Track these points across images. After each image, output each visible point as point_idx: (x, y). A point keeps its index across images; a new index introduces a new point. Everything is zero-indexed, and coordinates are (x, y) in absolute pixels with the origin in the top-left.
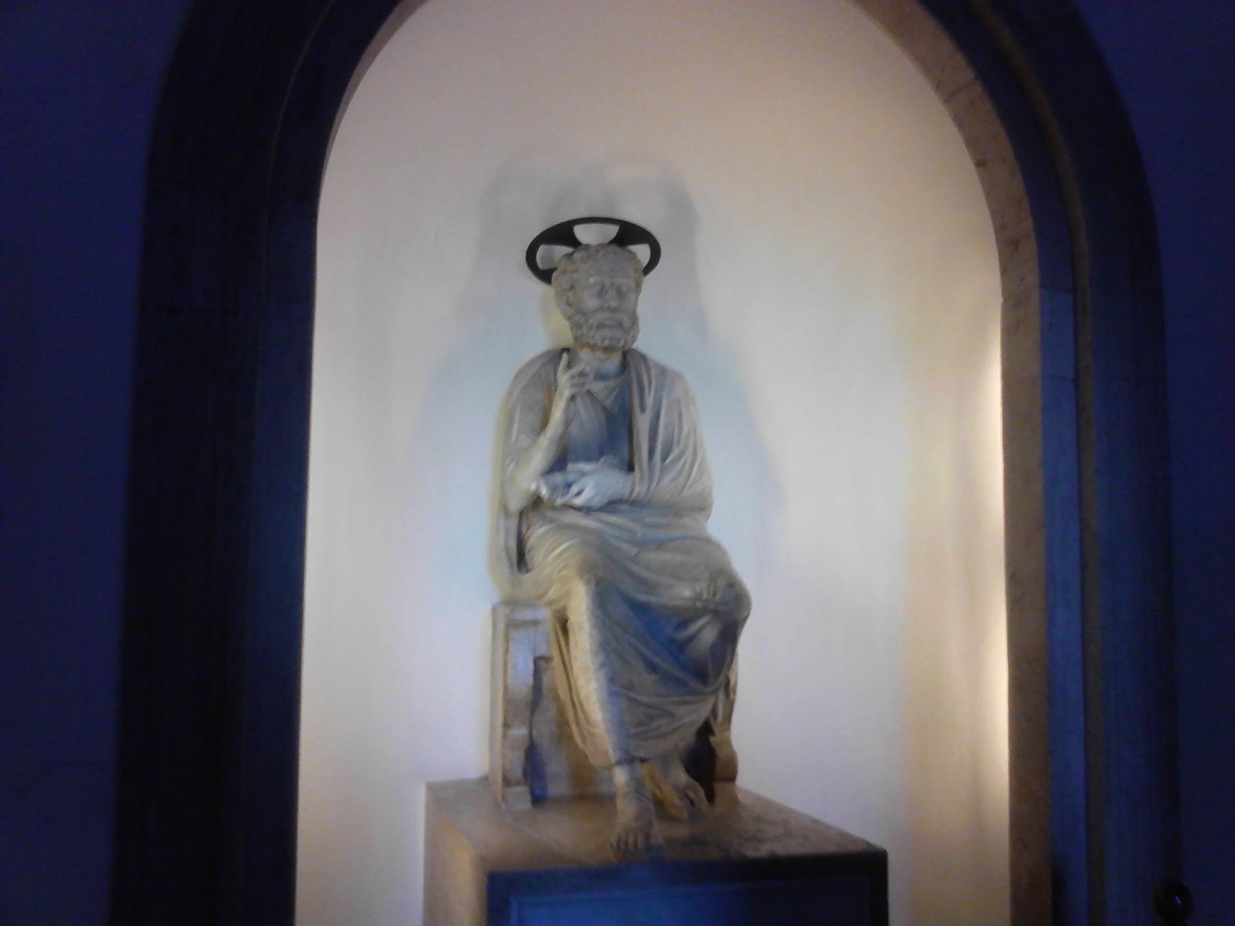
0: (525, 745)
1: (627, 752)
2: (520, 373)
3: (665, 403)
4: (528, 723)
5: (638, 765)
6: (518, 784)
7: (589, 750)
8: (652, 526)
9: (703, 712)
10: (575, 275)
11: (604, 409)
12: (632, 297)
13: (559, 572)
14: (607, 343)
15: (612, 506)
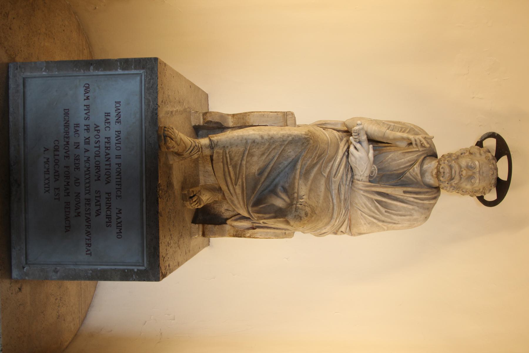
1: (216, 145)
3: (410, 207)
4: (234, 126)
6: (204, 119)
8: (339, 190)
10: (478, 155)
11: (403, 173)
14: (442, 170)
15: (350, 169)
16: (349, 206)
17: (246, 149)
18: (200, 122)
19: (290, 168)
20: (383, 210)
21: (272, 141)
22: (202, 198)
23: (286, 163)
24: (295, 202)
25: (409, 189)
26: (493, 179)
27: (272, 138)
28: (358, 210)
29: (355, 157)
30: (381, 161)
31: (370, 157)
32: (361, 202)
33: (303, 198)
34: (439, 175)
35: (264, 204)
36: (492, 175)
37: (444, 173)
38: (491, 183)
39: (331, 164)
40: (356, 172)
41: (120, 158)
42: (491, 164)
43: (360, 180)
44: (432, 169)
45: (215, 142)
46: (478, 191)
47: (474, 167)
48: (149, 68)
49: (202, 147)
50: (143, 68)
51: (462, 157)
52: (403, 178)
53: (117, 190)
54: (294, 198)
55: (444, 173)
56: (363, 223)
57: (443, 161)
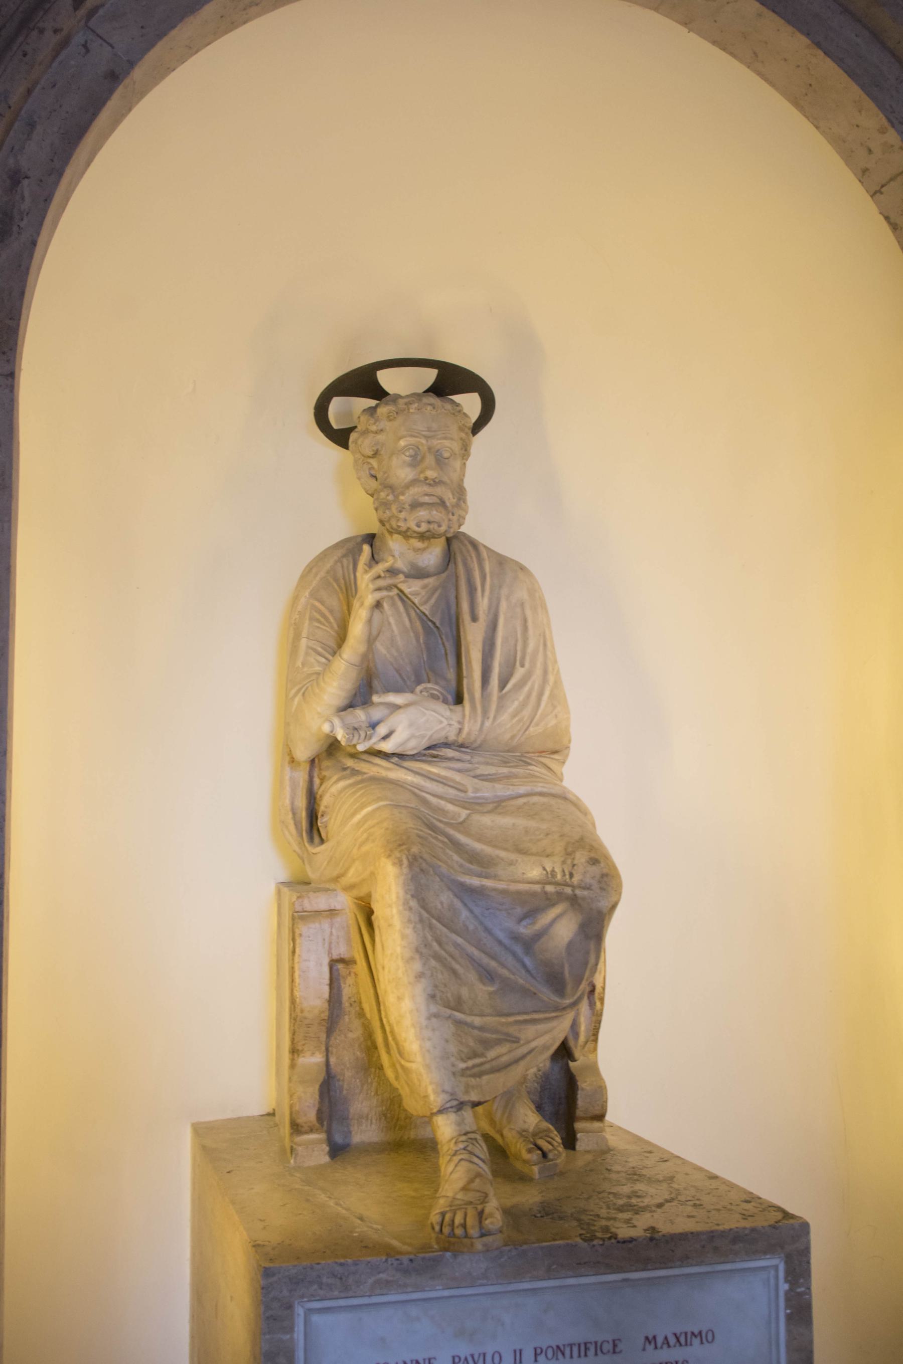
0: (322, 1076)
2: (309, 569)
4: (324, 1048)
5: (468, 1113)
6: (311, 1130)
7: (404, 1091)
9: (558, 1030)
10: (381, 437)
11: (423, 617)
12: (457, 464)
13: (360, 846)
14: (424, 527)
16: (514, 754)
17: (450, 1017)
18: (319, 1142)
19: (475, 902)
20: (519, 673)
21: (424, 951)
22: (534, 1125)
23: (465, 913)
24: (568, 890)
25: (465, 606)
26: (443, 407)
27: (417, 950)
28: (527, 732)
29: (408, 740)
30: (395, 673)
31: (406, 702)
32: (509, 725)
33: (553, 871)
34: (434, 534)
35: (562, 966)
36: (434, 408)
37: (429, 522)
38: (452, 411)
39: (434, 800)
40: (439, 737)
41: (521, 1351)
42: (409, 409)
43: (460, 727)
44: (409, 549)
45: (446, 1097)
46: (464, 443)
47: (412, 449)
48: (291, 1291)
49: (463, 1132)
50: (290, 1307)
51: (386, 475)
52: (434, 620)
53: (599, 1352)
54: (559, 894)
55: (429, 522)
56: (553, 722)
57: (401, 524)
